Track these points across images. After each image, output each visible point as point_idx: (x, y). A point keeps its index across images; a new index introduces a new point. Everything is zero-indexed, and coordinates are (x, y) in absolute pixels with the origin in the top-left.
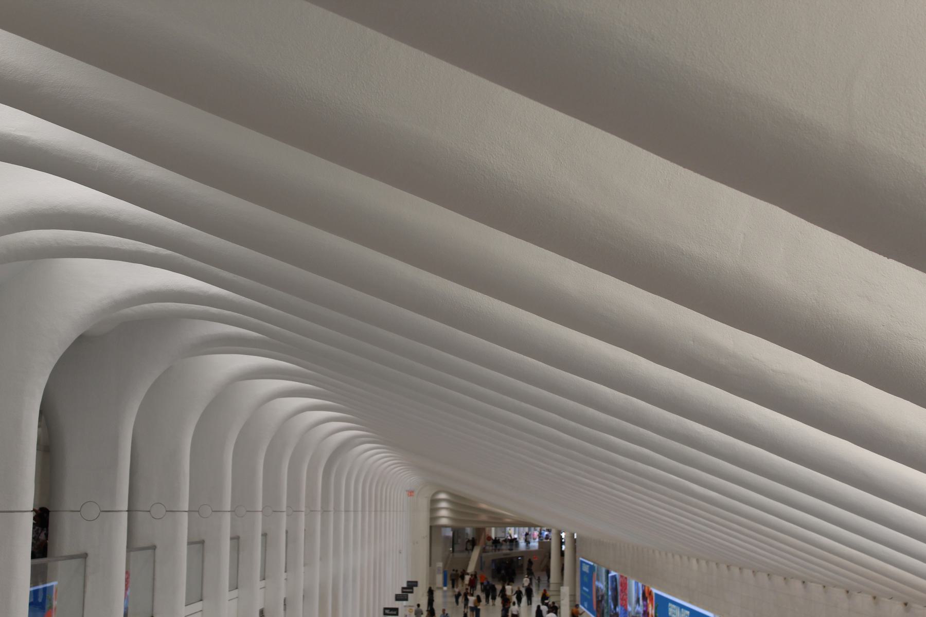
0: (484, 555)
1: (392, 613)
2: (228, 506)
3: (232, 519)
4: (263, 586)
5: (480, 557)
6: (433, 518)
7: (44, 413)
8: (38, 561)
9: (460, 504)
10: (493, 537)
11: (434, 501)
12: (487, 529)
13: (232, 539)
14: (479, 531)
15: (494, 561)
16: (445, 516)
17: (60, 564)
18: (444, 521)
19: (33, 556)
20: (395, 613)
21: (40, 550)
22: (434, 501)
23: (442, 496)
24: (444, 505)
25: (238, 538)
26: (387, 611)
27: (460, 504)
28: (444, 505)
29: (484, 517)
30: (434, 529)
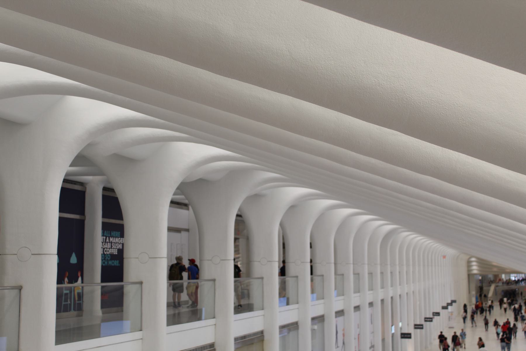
0: (497, 288)
1: (437, 314)
2: (351, 262)
3: (353, 267)
4: (141, 338)
5: (495, 290)
6: (469, 270)
7: (281, 225)
8: (60, 286)
9: (482, 263)
10: (505, 280)
11: (469, 262)
12: (500, 276)
13: (369, 274)
14: (496, 276)
15: (503, 291)
16: (475, 269)
17: (203, 283)
18: (475, 272)
19: (235, 277)
20: (438, 314)
21: (312, 274)
22: (469, 262)
23: (473, 259)
24: (474, 263)
25: (371, 273)
26: (434, 314)
27: (482, 263)
28: (474, 263)
29: (495, 269)
30: (470, 276)
